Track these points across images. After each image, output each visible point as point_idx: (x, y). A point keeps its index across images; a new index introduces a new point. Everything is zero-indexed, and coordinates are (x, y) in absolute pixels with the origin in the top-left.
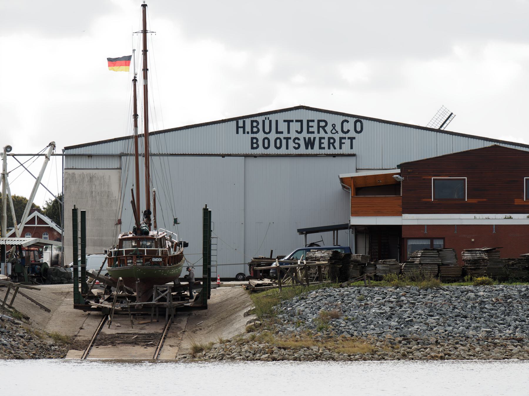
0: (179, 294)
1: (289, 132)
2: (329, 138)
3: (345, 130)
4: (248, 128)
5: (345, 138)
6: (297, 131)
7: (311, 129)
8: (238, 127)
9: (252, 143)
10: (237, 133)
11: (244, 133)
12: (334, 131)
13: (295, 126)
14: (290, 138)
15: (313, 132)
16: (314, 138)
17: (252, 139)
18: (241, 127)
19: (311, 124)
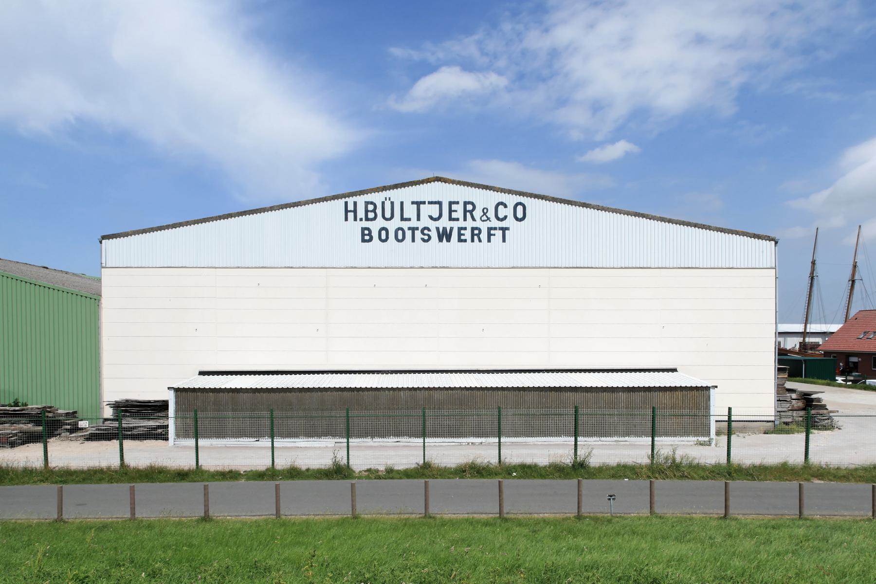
0: (847, 362)
1: (418, 219)
2: (473, 229)
3: (501, 216)
4: (361, 213)
5: (495, 229)
6: (431, 217)
7: (454, 215)
8: (347, 211)
9: (363, 235)
10: (346, 219)
11: (355, 219)
12: (484, 218)
13: (426, 210)
14: (417, 229)
15: (458, 219)
16: (452, 229)
17: (363, 229)
18: (351, 211)
19: (454, 207)
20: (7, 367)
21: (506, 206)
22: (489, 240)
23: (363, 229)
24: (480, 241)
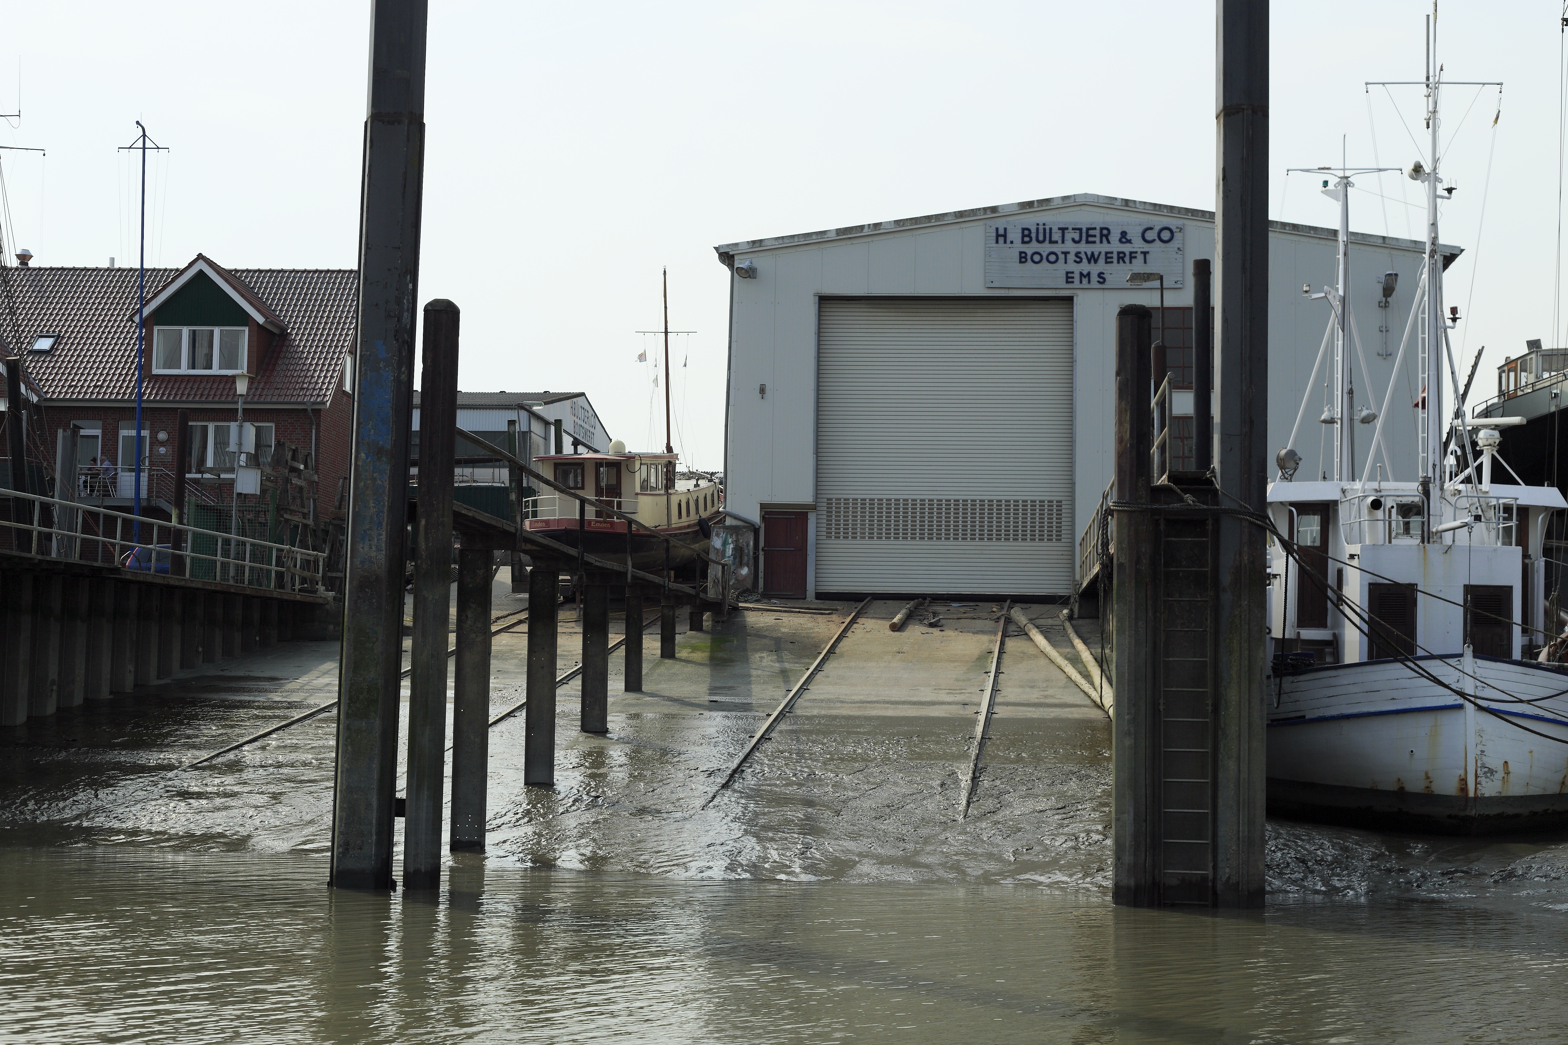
8: (998, 236)
11: (1005, 242)
13: (1069, 236)
17: (1021, 253)
18: (1001, 236)
19: (1091, 232)
20: (303, 870)
21: (1073, 240)
22: (1131, 262)
23: (1021, 253)
24: (1124, 262)
